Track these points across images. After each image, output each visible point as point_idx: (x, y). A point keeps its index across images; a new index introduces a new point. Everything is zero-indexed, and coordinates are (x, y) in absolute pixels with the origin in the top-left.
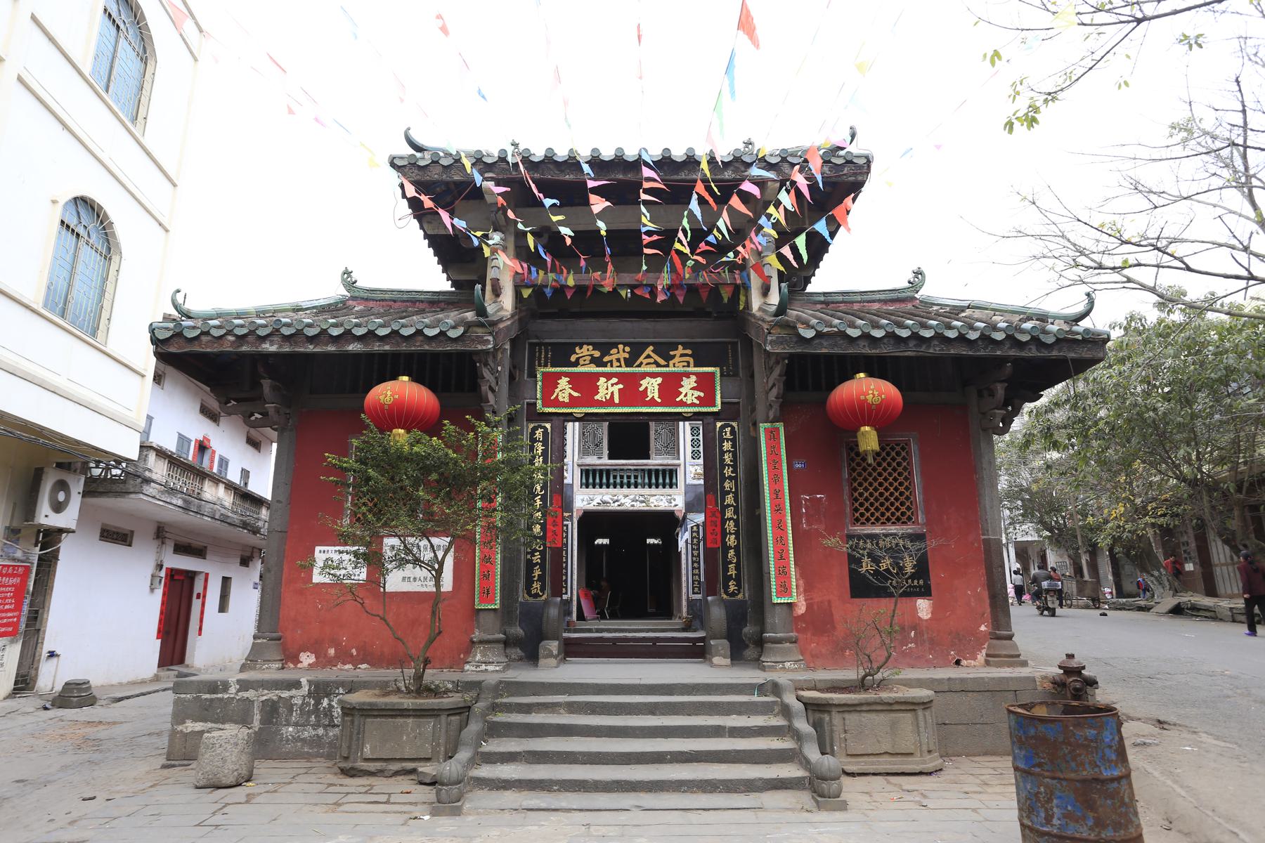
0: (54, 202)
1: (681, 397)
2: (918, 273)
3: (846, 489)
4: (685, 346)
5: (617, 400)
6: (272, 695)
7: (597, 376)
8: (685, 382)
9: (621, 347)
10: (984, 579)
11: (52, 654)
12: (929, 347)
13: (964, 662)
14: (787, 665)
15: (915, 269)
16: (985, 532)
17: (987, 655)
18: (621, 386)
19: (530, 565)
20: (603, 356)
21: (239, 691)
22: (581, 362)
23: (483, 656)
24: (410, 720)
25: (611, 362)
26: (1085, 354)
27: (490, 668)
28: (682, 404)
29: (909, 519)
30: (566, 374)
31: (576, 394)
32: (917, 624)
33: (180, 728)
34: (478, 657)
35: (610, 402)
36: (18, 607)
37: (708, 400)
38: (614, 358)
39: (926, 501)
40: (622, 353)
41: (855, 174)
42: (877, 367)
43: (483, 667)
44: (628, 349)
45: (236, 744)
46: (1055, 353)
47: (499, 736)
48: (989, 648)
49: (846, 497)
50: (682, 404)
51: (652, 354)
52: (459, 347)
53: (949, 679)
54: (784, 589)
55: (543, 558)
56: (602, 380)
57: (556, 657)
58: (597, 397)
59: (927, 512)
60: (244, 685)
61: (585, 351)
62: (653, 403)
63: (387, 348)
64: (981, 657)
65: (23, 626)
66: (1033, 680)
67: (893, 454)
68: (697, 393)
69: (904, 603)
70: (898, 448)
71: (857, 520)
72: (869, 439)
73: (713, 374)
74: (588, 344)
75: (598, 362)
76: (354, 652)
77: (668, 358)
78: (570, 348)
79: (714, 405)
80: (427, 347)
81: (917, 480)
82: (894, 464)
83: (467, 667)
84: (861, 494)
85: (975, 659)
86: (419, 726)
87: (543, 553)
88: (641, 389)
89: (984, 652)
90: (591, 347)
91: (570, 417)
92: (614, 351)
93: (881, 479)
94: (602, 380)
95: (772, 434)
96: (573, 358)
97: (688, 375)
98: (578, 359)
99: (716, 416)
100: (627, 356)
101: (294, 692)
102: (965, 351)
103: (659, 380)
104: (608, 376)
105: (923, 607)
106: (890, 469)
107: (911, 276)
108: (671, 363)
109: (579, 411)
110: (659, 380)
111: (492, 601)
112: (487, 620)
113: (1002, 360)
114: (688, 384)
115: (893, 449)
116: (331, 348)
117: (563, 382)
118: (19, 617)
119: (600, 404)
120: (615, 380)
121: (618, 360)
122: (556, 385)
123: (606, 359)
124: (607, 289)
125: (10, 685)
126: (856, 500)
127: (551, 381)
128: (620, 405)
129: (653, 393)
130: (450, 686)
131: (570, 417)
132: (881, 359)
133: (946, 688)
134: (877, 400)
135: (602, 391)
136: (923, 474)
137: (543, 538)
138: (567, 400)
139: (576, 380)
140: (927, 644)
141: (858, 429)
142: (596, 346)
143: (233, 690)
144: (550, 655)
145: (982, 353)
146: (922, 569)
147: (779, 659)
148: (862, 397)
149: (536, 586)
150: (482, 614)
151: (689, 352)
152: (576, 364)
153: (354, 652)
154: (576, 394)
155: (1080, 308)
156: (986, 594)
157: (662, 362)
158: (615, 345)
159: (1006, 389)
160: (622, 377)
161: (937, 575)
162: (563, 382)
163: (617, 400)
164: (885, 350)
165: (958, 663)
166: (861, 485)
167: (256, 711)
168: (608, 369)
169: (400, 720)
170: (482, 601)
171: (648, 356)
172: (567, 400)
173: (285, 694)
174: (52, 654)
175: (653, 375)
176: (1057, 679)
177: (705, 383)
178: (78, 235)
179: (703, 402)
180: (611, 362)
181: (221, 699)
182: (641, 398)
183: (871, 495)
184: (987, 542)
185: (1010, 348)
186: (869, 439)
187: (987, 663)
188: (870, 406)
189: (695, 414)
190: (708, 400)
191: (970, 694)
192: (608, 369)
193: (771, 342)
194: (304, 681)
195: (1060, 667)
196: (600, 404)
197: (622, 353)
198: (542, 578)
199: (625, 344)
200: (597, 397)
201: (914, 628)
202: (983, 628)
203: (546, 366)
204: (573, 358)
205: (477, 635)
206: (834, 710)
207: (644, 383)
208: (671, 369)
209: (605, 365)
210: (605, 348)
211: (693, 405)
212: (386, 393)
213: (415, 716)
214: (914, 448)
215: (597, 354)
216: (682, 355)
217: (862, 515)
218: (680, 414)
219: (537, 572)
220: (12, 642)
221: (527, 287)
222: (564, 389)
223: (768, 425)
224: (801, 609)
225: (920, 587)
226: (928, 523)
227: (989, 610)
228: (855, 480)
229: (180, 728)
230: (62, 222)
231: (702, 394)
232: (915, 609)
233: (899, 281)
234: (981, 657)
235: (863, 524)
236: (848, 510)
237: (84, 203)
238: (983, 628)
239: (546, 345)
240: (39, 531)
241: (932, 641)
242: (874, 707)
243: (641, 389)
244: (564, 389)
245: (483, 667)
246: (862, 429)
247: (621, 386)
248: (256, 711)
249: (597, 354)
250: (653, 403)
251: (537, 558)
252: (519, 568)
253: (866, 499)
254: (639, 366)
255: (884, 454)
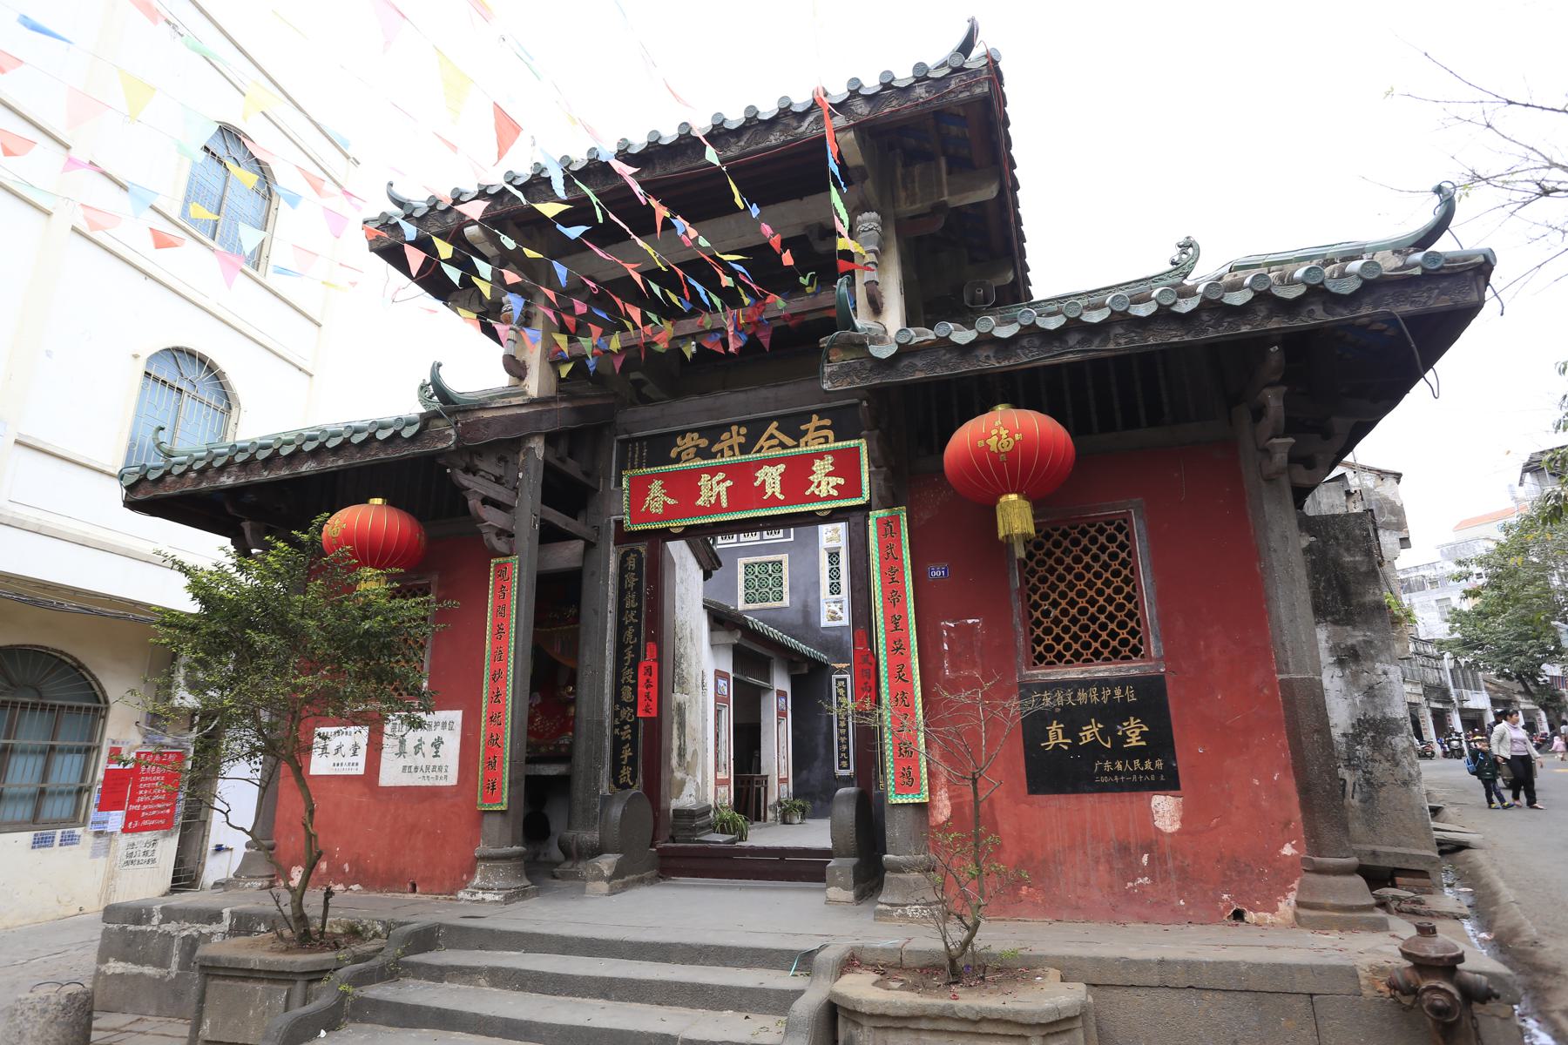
0: (136, 356)
1: (812, 488)
2: (1186, 246)
3: (1017, 607)
4: (822, 414)
5: (724, 504)
6: (191, 930)
7: (697, 473)
8: (818, 465)
9: (734, 428)
10: (1286, 756)
11: (219, 849)
12: (1106, 340)
13: (1250, 916)
14: (909, 910)
15: (1182, 240)
16: (1283, 667)
17: (1299, 904)
18: (729, 483)
19: (617, 744)
20: (712, 444)
21: (162, 922)
22: (684, 456)
23: (483, 879)
24: (259, 987)
25: (722, 451)
26: (1437, 300)
27: (489, 897)
28: (815, 498)
29: (1135, 651)
30: (659, 476)
31: (671, 502)
32: (1152, 841)
33: (103, 968)
34: (477, 881)
35: (716, 508)
36: (171, 796)
37: (852, 489)
38: (725, 445)
39: (1164, 618)
40: (737, 436)
41: (968, 87)
42: (1020, 389)
43: (480, 895)
44: (743, 431)
45: (45, 1011)
46: (1365, 311)
47: (363, 1021)
48: (1300, 891)
49: (1016, 620)
50: (815, 498)
51: (777, 433)
52: (416, 450)
53: (1162, 962)
54: (908, 781)
55: (634, 733)
56: (705, 477)
57: (609, 880)
58: (700, 502)
59: (1166, 636)
60: (169, 915)
61: (691, 441)
62: (773, 501)
63: (341, 462)
64: (1287, 906)
65: (179, 820)
66: (1352, 973)
67: (1102, 539)
68: (834, 481)
69: (1128, 801)
70: (1110, 530)
71: (1041, 658)
72: (1015, 516)
73: (857, 449)
74: (692, 431)
75: (703, 453)
76: (346, 866)
77: (797, 436)
78: (669, 439)
79: (859, 494)
80: (382, 456)
81: (1145, 580)
82: (1105, 557)
83: (461, 894)
84: (1046, 614)
85: (1273, 910)
86: (270, 996)
87: (634, 726)
88: (757, 484)
89: (1292, 897)
90: (696, 435)
91: (667, 535)
92: (725, 436)
93: (1081, 585)
94: (705, 477)
95: (888, 527)
96: (673, 454)
97: (820, 455)
98: (679, 454)
99: (866, 508)
100: (742, 440)
101: (214, 927)
102: (1175, 337)
103: (782, 467)
104: (712, 471)
105: (1165, 810)
106: (1097, 567)
107: (1174, 253)
108: (802, 441)
109: (676, 524)
110: (782, 467)
111: (498, 800)
112: (493, 826)
113: (1260, 341)
114: (821, 467)
115: (1101, 531)
116: (284, 473)
117: (656, 487)
118: (173, 808)
119: (704, 511)
120: (721, 476)
121: (731, 448)
122: (646, 492)
123: (715, 448)
124: (662, 347)
125: (167, 882)
126: (1038, 623)
127: (640, 489)
128: (729, 510)
129: (774, 487)
130: (379, 928)
131: (667, 535)
132: (1032, 373)
133: (1156, 980)
134: (1007, 445)
135: (704, 492)
136: (1157, 570)
137: (634, 705)
138: (660, 511)
139: (671, 483)
140: (1173, 877)
141: (996, 501)
142: (702, 432)
143: (155, 921)
144: (600, 877)
145: (1211, 334)
146: (1160, 743)
147: (896, 901)
148: (981, 444)
149: (626, 771)
150: (487, 819)
151: (827, 422)
152: (678, 460)
153: (346, 866)
154: (671, 502)
155: (1425, 216)
156: (1291, 787)
157: (788, 441)
158: (726, 427)
159: (1287, 400)
160: (730, 470)
161: (1189, 751)
162: (656, 487)
163: (724, 504)
164: (1023, 358)
165: (1238, 915)
166: (1045, 597)
167: (175, 951)
168: (718, 461)
169: (249, 985)
170: (486, 799)
171: (772, 437)
172: (660, 511)
173: (206, 929)
174: (219, 849)
175: (773, 462)
176: (1399, 977)
177: (846, 465)
178: (180, 390)
179: (844, 492)
180: (722, 451)
181: (144, 933)
182: (756, 496)
183: (1064, 612)
184: (1287, 685)
185: (1269, 317)
186: (1015, 516)
187: (1298, 921)
188: (995, 456)
189: (834, 510)
190: (852, 489)
191: (1208, 996)
192: (718, 461)
193: (831, 374)
194: (226, 912)
195: (1406, 955)
196: (704, 511)
197: (737, 436)
198: (632, 761)
199: (740, 424)
200: (700, 502)
201: (1148, 848)
202: (1288, 850)
203: (640, 467)
204: (673, 454)
205: (482, 849)
206: (864, 1022)
207: (760, 474)
208: (802, 450)
209: (714, 456)
210: (713, 433)
211: (830, 498)
212: (339, 522)
213: (269, 980)
214: (1137, 526)
215: (704, 443)
216: (818, 429)
217: (1049, 648)
218: (812, 513)
219: (627, 753)
220: (165, 836)
221: (566, 361)
222: (657, 497)
223: (882, 513)
224: (943, 811)
225: (1157, 773)
226: (1167, 657)
227: (1299, 816)
228: (1034, 590)
229: (103, 968)
230: (147, 374)
231: (841, 481)
232: (1148, 815)
233: (1156, 261)
234: (1287, 906)
235: (1051, 663)
236: (1021, 641)
237: (181, 355)
238: (1288, 850)
239: (640, 439)
240: (194, 715)
241: (1182, 872)
242: (941, 1025)
243: (757, 484)
244: (657, 497)
245: (480, 895)
246: (1003, 499)
247: (729, 483)
248: (175, 951)
249: (704, 443)
250: (773, 501)
251: (626, 734)
252: (601, 748)
253: (1057, 622)
254: (759, 451)
255: (1049, 545)
